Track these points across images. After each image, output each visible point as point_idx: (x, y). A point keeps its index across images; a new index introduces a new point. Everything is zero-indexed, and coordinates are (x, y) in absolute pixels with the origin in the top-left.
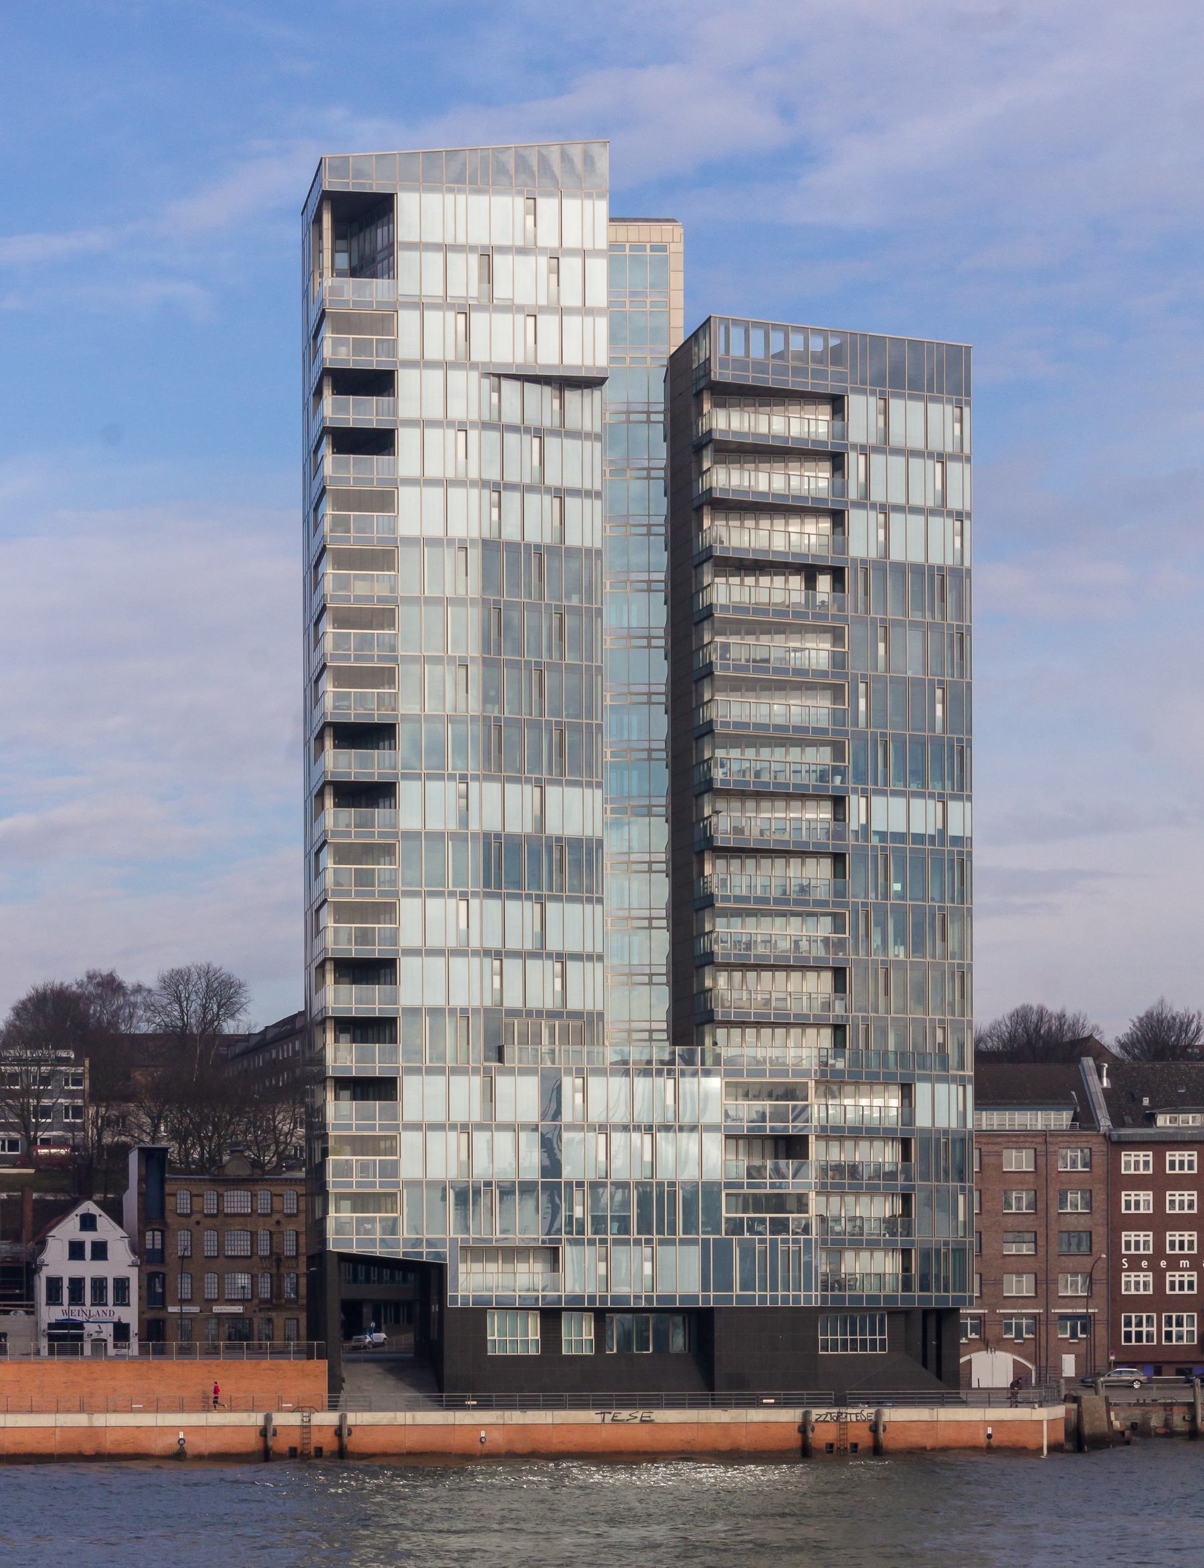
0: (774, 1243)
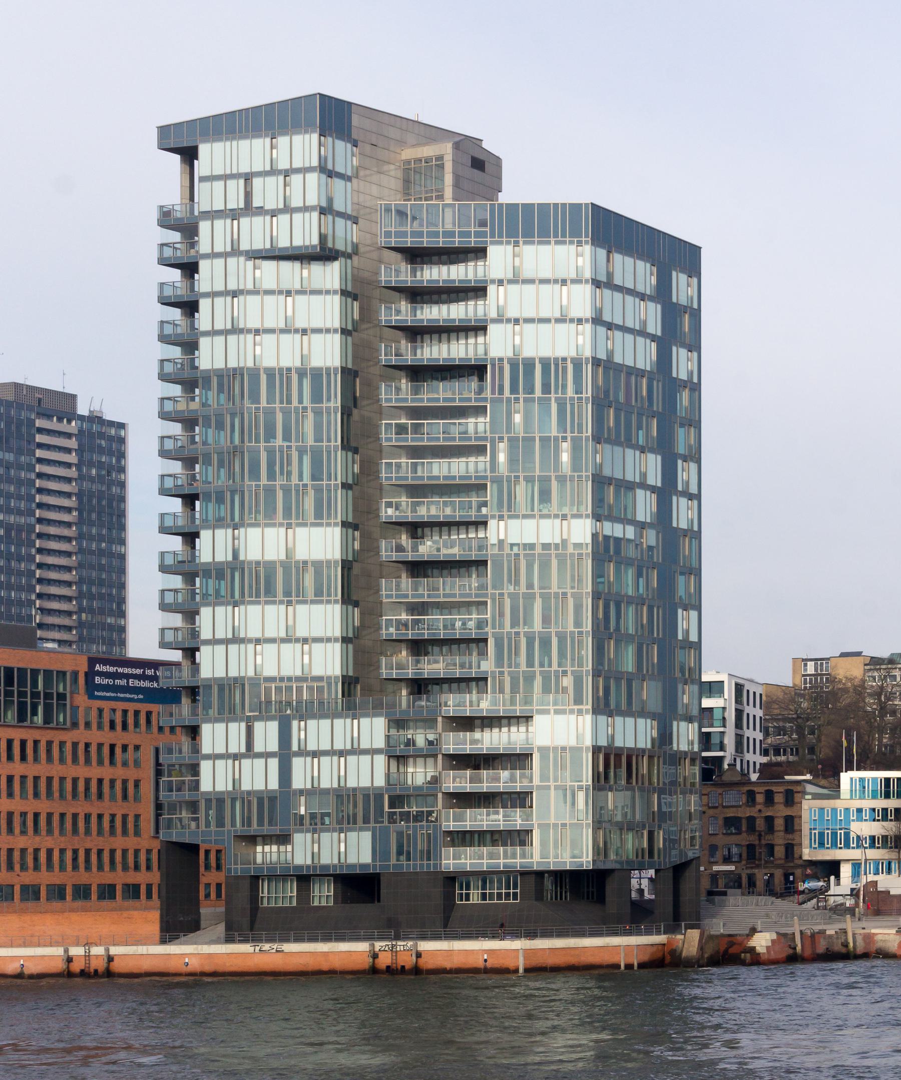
0: (415, 828)
